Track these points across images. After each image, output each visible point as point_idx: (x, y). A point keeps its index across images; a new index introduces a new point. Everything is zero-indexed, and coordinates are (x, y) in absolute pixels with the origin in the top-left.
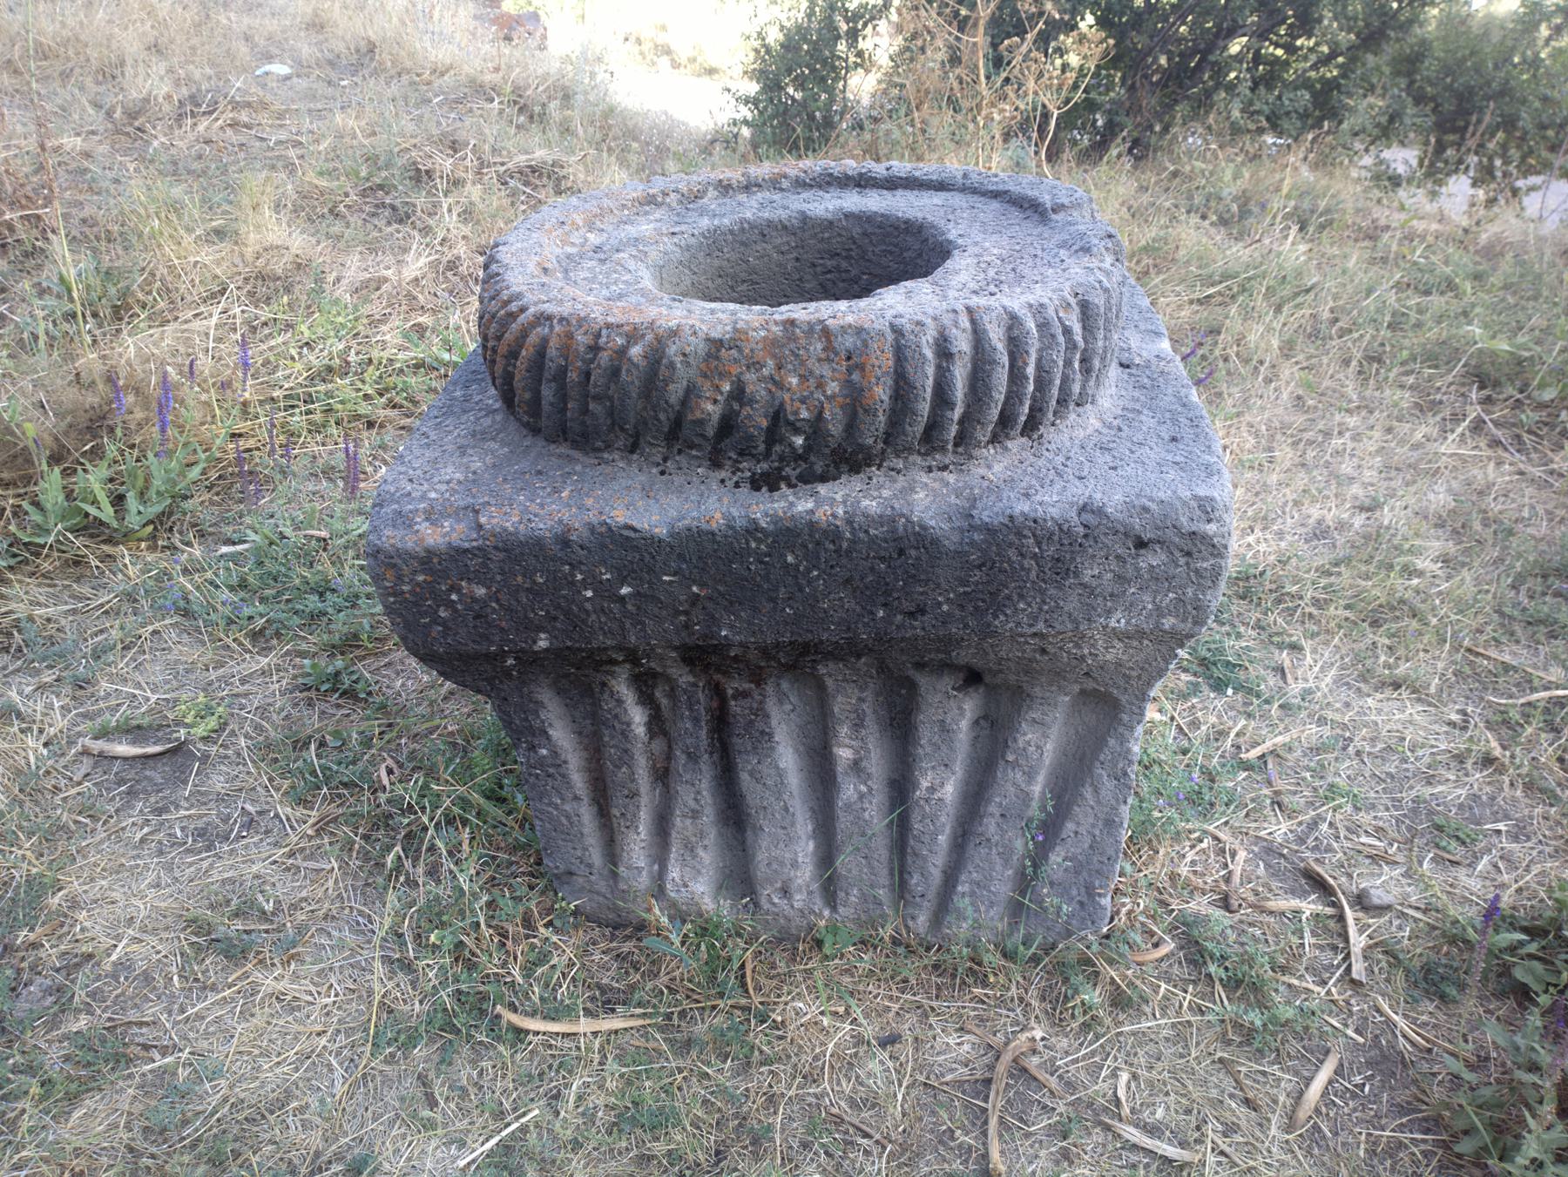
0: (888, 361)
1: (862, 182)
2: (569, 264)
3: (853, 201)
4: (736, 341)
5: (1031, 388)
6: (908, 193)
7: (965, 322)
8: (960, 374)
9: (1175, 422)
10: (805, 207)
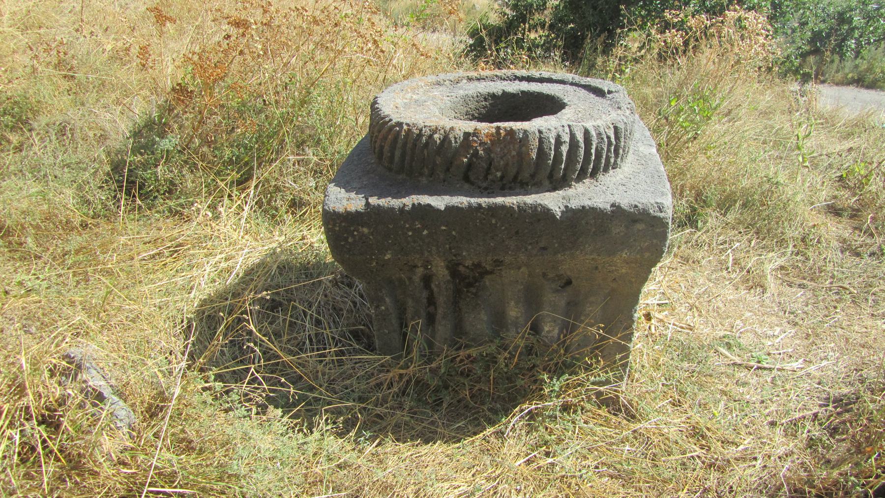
0: (536, 143)
1: (529, 79)
2: (407, 106)
3: (525, 86)
4: (476, 133)
5: (593, 158)
6: (549, 84)
7: (567, 130)
8: (565, 149)
9: (653, 177)
10: (504, 88)
